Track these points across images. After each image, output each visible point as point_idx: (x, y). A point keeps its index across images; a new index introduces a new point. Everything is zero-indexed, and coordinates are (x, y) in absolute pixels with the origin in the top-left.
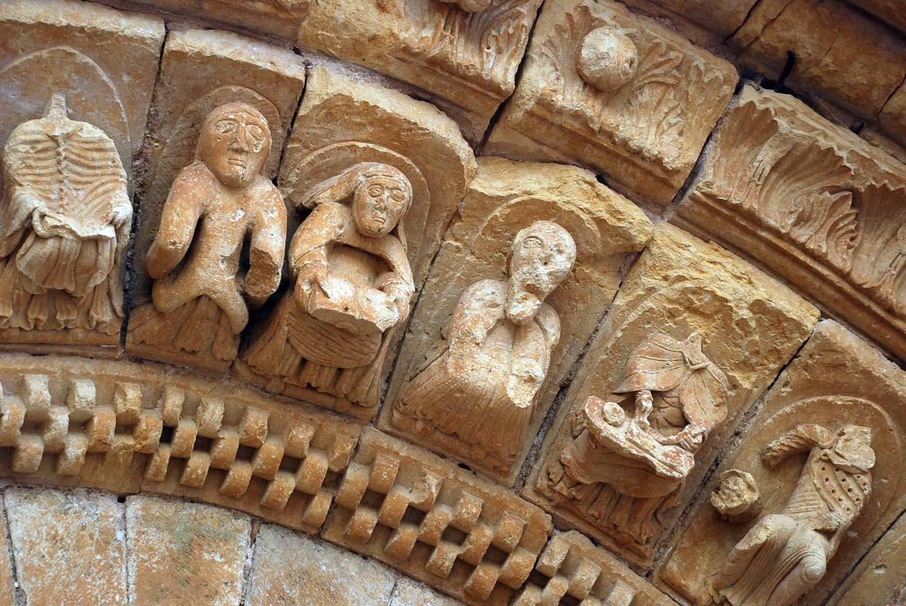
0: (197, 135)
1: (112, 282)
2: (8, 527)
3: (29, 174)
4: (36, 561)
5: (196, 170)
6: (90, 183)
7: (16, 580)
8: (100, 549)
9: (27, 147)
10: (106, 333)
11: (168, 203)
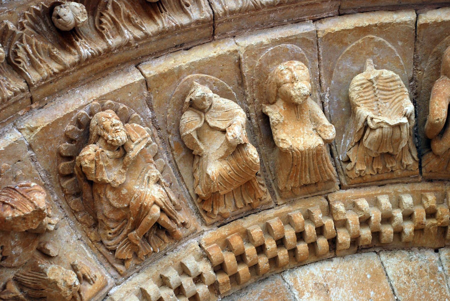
0: (440, 63)
1: (410, 144)
2: (385, 270)
3: (362, 100)
4: (402, 286)
5: (443, 80)
6: (391, 98)
7: (395, 296)
8: (432, 277)
9: (359, 88)
10: (412, 170)
11: (431, 100)
